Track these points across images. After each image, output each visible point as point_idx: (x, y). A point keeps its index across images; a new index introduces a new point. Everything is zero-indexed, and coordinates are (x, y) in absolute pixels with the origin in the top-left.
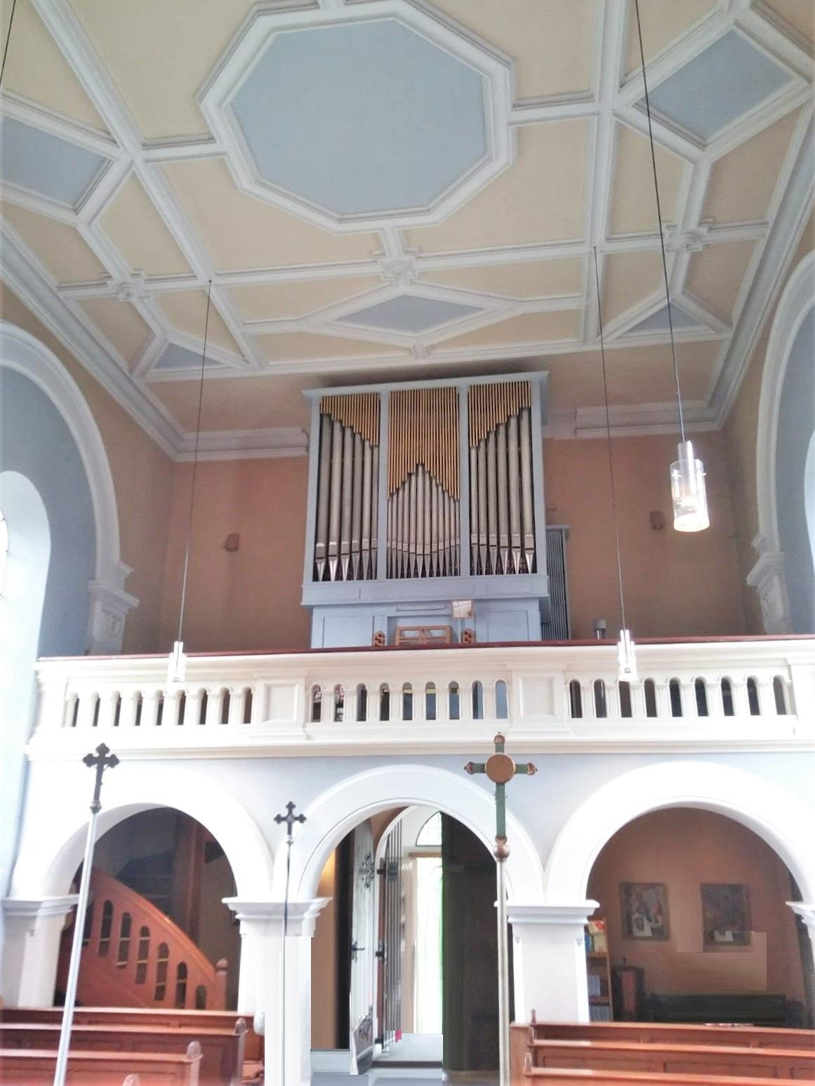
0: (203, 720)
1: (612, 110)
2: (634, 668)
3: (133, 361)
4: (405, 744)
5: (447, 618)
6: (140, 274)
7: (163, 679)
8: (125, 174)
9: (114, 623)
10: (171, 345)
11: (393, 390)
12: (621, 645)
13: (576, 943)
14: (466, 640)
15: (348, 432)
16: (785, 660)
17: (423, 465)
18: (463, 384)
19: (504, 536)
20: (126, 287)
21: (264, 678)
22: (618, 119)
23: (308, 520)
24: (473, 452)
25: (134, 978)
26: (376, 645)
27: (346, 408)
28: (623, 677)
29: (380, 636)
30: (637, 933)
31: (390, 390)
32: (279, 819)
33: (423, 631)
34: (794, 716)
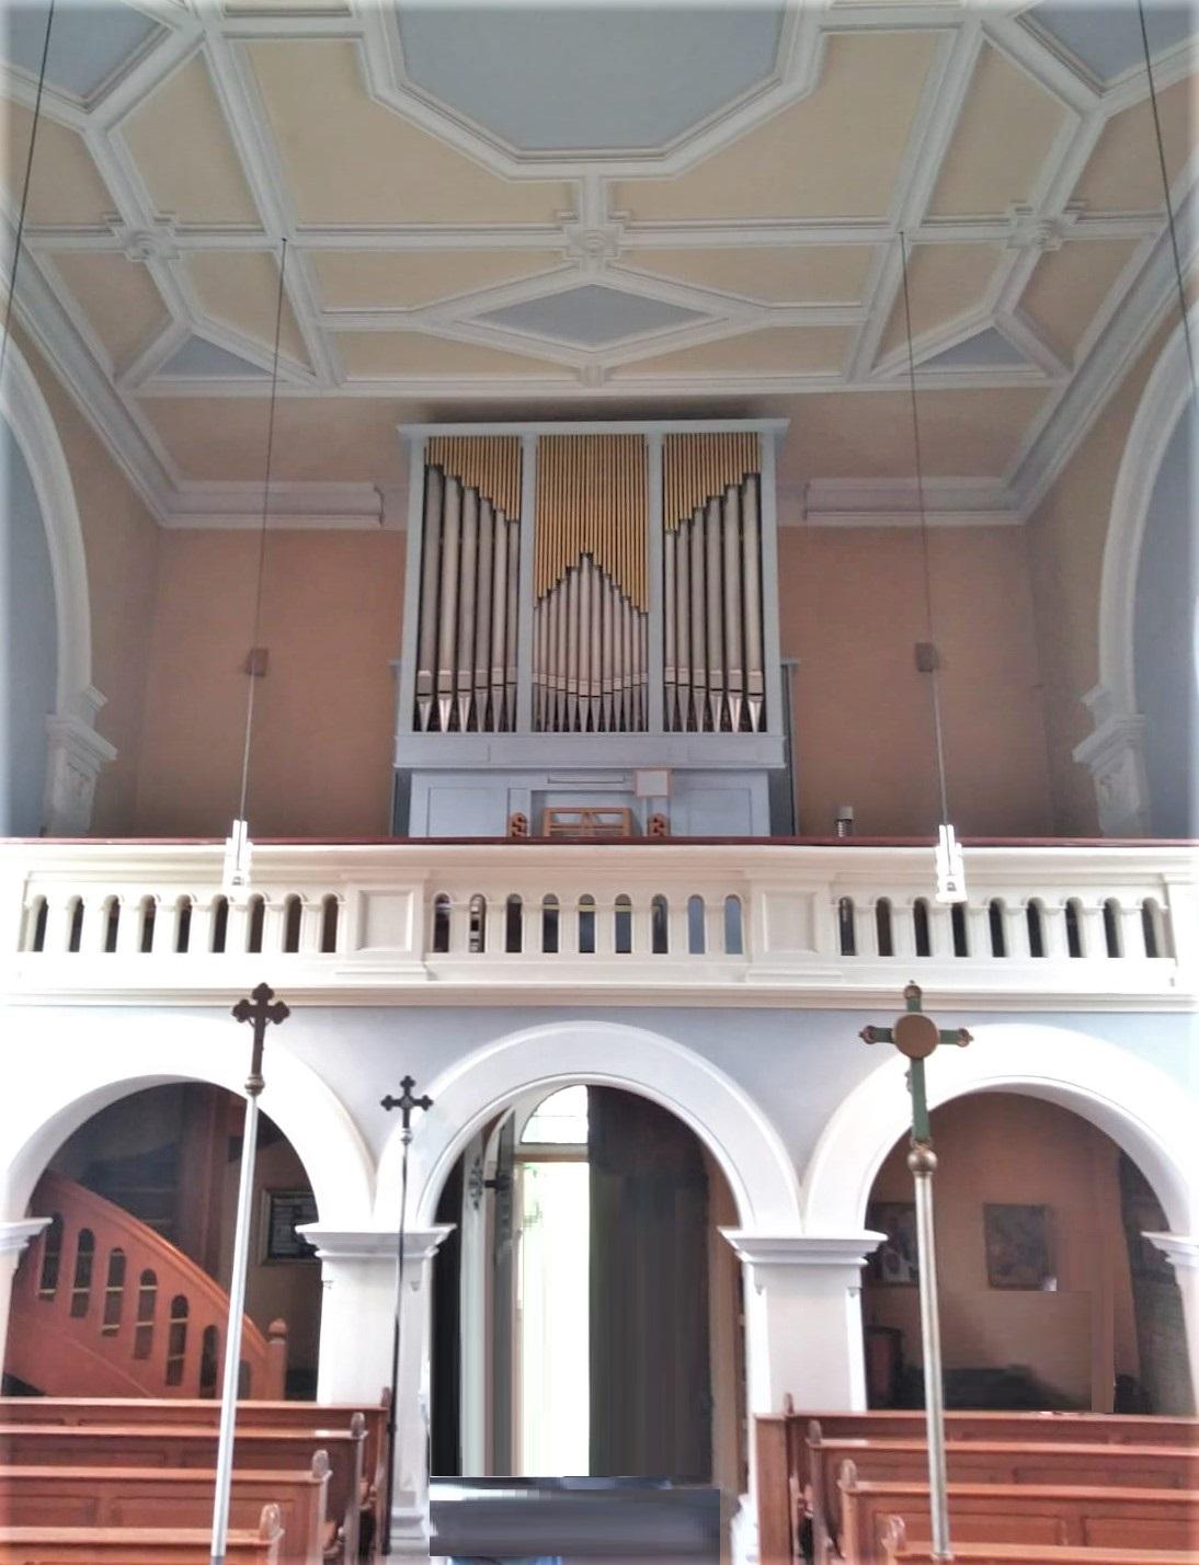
0: (74, 945)
1: (982, 22)
2: (960, 882)
3: (124, 359)
4: (657, 990)
5: (625, 797)
6: (168, 220)
7: (216, 878)
8: (185, 54)
9: (81, 784)
10: (196, 339)
11: (543, 434)
12: (940, 851)
13: (847, 1293)
14: (656, 831)
15: (470, 497)
16: (1160, 876)
17: (590, 556)
18: (655, 430)
19: (716, 672)
20: (148, 240)
21: (357, 881)
22: (987, 38)
23: (405, 628)
24: (670, 539)
25: (131, 1350)
26: (514, 834)
27: (465, 457)
28: (227, 890)
29: (520, 820)
30: (889, 1276)
31: (666, 432)
32: (388, 1103)
33: (587, 814)
34: (1172, 960)
